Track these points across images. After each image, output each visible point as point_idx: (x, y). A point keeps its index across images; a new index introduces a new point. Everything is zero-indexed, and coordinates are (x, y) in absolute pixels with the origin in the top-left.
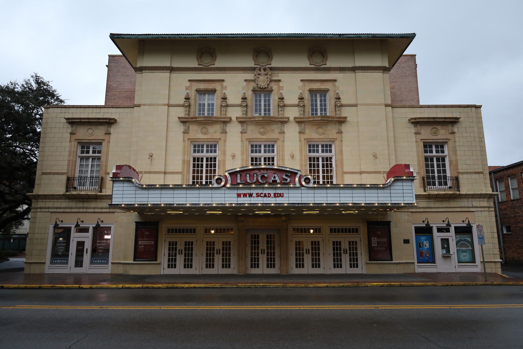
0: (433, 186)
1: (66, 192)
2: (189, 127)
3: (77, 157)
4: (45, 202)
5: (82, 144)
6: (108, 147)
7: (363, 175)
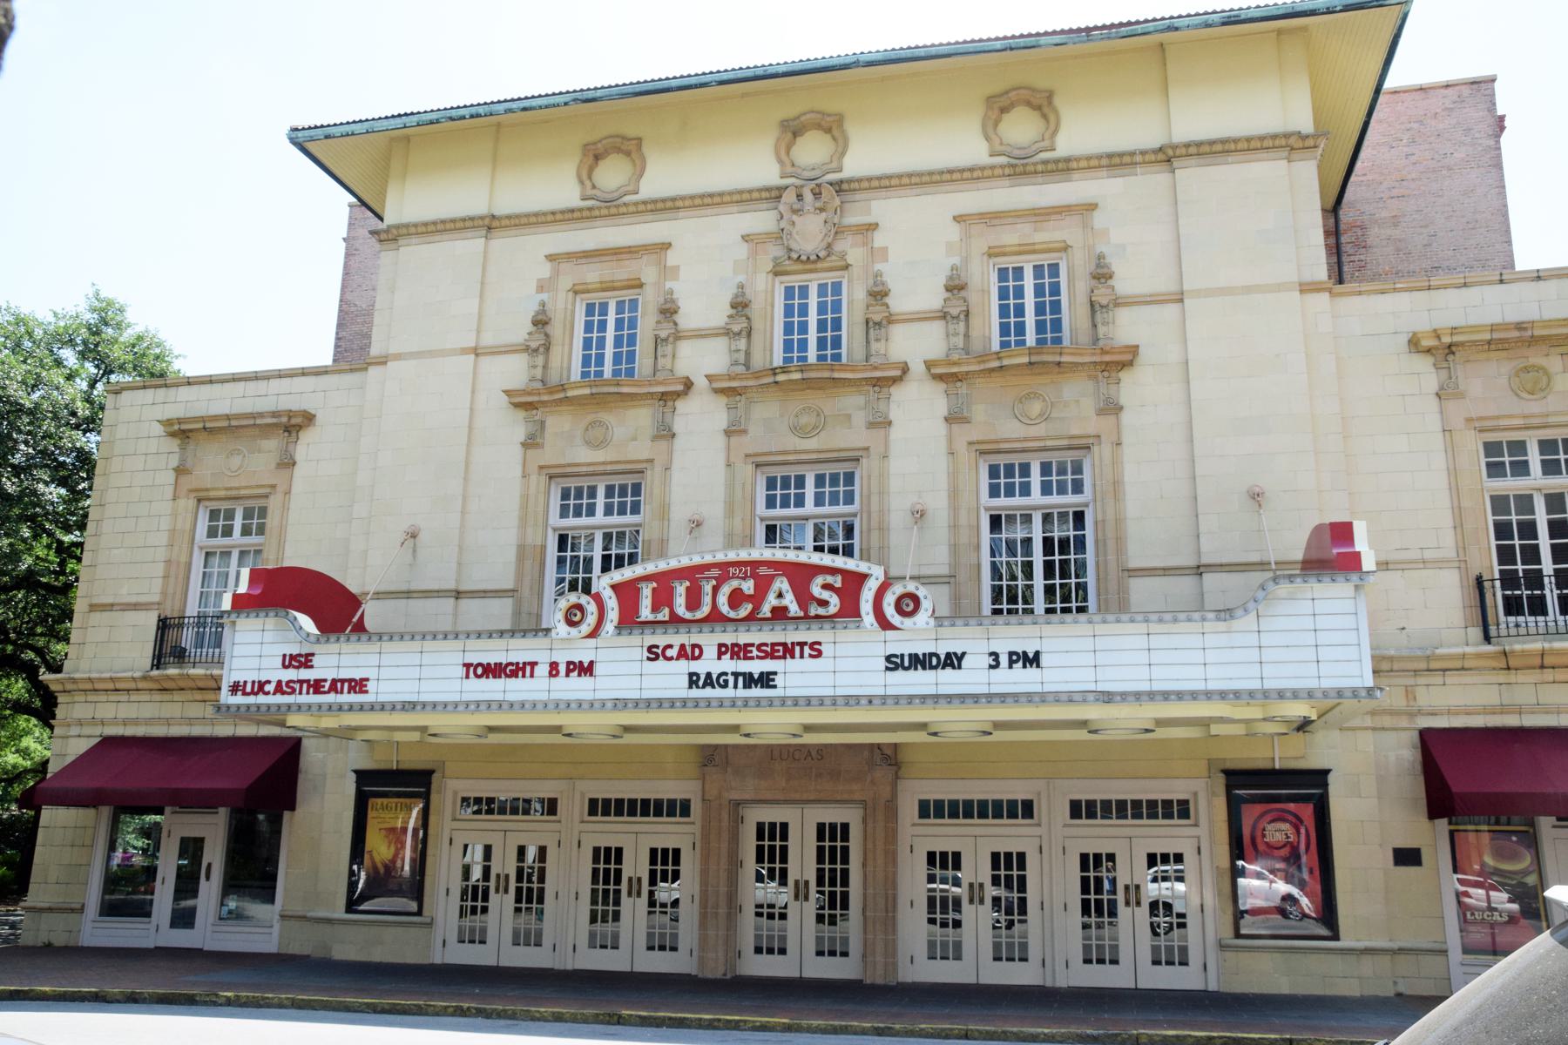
0: (1533, 618)
1: (152, 669)
2: (543, 423)
3: (757, 519)
6: (285, 508)
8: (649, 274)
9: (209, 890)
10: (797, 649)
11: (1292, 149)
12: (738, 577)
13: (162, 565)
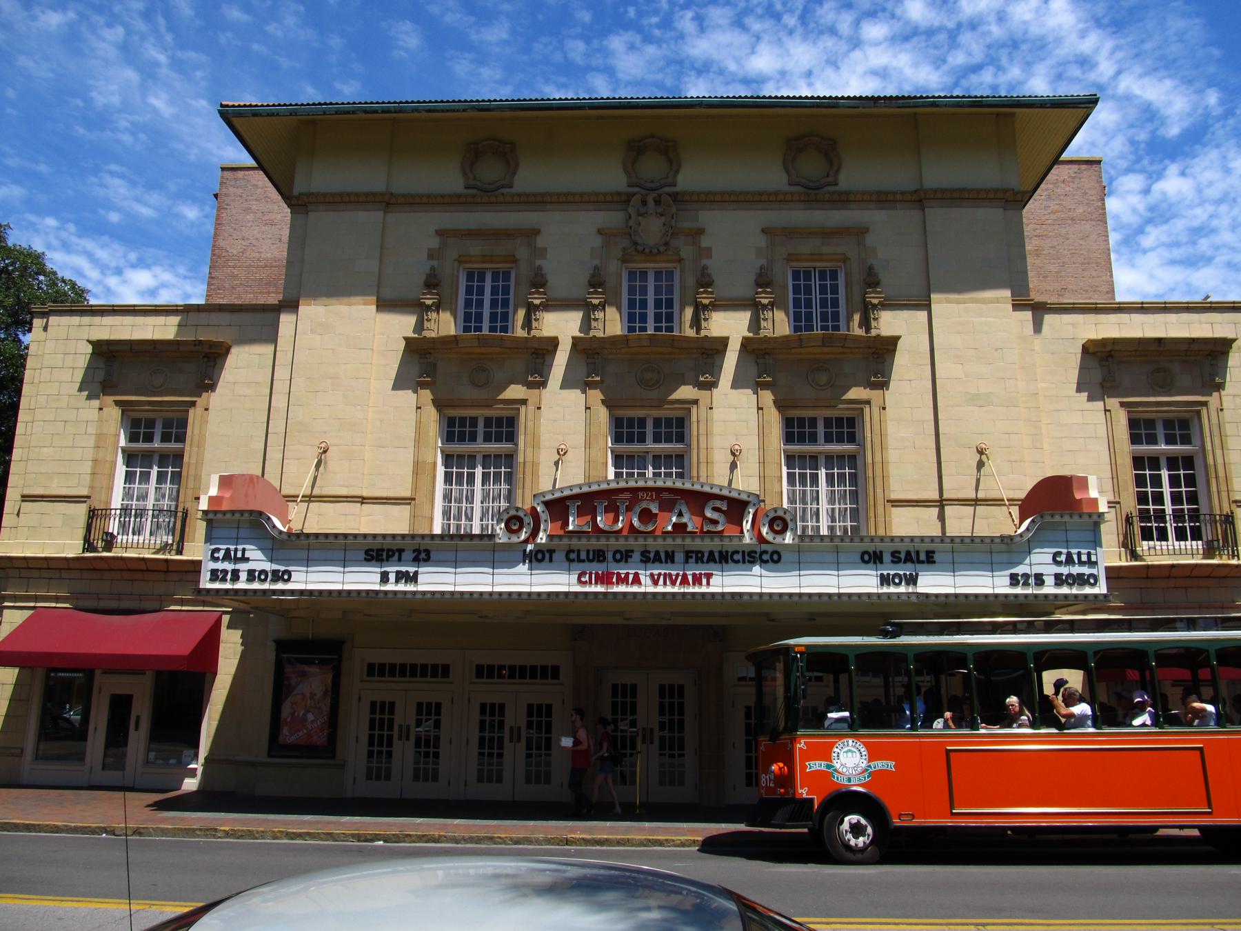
4: (26, 580)
8: (522, 252)
9: (138, 739)
11: (1007, 201)
12: (646, 499)
13: (90, 463)
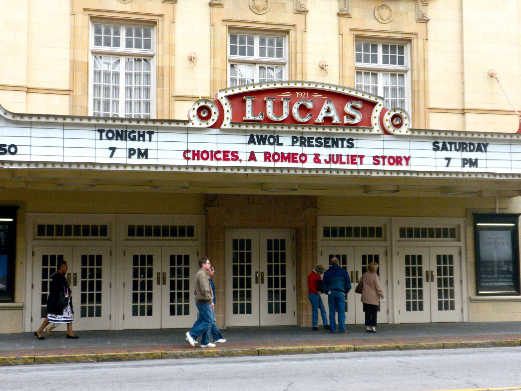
5: (384, 41)
7: (33, 96)
10: (340, 142)
